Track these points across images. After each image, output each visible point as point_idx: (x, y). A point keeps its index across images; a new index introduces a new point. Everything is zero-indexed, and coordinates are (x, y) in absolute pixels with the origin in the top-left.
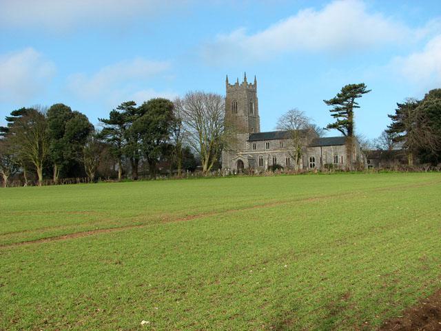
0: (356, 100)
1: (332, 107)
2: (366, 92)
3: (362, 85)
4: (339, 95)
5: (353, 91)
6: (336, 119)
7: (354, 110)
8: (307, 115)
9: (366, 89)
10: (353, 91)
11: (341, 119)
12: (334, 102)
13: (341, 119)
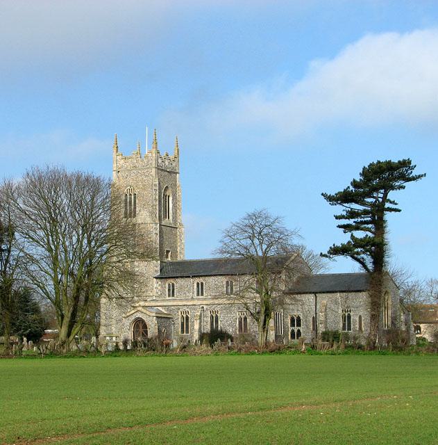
0: (392, 195)
1: (340, 209)
2: (414, 179)
3: (406, 164)
4: (355, 184)
5: (384, 177)
6: (349, 234)
7: (388, 216)
8: (288, 224)
9: (415, 173)
10: (384, 177)
11: (359, 234)
12: (344, 197)
13: (359, 234)
